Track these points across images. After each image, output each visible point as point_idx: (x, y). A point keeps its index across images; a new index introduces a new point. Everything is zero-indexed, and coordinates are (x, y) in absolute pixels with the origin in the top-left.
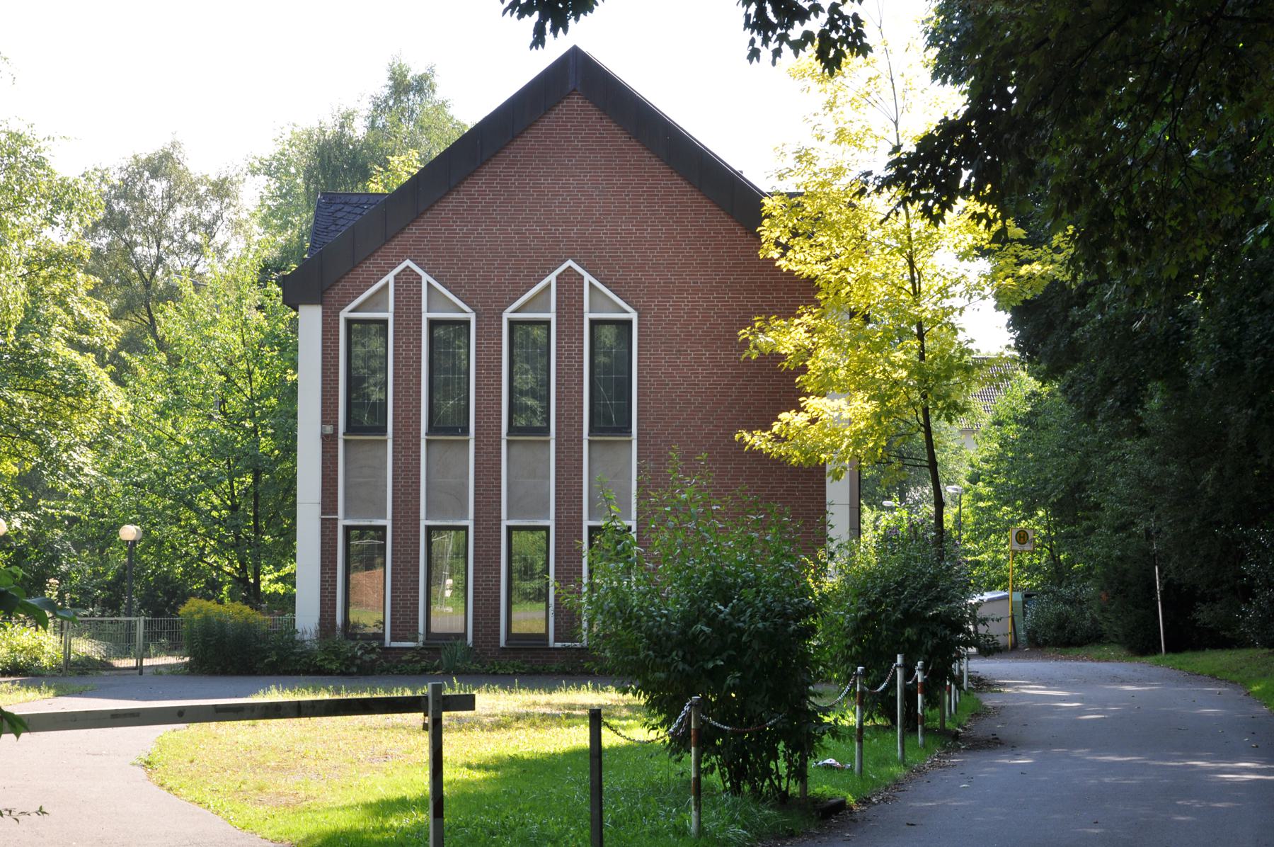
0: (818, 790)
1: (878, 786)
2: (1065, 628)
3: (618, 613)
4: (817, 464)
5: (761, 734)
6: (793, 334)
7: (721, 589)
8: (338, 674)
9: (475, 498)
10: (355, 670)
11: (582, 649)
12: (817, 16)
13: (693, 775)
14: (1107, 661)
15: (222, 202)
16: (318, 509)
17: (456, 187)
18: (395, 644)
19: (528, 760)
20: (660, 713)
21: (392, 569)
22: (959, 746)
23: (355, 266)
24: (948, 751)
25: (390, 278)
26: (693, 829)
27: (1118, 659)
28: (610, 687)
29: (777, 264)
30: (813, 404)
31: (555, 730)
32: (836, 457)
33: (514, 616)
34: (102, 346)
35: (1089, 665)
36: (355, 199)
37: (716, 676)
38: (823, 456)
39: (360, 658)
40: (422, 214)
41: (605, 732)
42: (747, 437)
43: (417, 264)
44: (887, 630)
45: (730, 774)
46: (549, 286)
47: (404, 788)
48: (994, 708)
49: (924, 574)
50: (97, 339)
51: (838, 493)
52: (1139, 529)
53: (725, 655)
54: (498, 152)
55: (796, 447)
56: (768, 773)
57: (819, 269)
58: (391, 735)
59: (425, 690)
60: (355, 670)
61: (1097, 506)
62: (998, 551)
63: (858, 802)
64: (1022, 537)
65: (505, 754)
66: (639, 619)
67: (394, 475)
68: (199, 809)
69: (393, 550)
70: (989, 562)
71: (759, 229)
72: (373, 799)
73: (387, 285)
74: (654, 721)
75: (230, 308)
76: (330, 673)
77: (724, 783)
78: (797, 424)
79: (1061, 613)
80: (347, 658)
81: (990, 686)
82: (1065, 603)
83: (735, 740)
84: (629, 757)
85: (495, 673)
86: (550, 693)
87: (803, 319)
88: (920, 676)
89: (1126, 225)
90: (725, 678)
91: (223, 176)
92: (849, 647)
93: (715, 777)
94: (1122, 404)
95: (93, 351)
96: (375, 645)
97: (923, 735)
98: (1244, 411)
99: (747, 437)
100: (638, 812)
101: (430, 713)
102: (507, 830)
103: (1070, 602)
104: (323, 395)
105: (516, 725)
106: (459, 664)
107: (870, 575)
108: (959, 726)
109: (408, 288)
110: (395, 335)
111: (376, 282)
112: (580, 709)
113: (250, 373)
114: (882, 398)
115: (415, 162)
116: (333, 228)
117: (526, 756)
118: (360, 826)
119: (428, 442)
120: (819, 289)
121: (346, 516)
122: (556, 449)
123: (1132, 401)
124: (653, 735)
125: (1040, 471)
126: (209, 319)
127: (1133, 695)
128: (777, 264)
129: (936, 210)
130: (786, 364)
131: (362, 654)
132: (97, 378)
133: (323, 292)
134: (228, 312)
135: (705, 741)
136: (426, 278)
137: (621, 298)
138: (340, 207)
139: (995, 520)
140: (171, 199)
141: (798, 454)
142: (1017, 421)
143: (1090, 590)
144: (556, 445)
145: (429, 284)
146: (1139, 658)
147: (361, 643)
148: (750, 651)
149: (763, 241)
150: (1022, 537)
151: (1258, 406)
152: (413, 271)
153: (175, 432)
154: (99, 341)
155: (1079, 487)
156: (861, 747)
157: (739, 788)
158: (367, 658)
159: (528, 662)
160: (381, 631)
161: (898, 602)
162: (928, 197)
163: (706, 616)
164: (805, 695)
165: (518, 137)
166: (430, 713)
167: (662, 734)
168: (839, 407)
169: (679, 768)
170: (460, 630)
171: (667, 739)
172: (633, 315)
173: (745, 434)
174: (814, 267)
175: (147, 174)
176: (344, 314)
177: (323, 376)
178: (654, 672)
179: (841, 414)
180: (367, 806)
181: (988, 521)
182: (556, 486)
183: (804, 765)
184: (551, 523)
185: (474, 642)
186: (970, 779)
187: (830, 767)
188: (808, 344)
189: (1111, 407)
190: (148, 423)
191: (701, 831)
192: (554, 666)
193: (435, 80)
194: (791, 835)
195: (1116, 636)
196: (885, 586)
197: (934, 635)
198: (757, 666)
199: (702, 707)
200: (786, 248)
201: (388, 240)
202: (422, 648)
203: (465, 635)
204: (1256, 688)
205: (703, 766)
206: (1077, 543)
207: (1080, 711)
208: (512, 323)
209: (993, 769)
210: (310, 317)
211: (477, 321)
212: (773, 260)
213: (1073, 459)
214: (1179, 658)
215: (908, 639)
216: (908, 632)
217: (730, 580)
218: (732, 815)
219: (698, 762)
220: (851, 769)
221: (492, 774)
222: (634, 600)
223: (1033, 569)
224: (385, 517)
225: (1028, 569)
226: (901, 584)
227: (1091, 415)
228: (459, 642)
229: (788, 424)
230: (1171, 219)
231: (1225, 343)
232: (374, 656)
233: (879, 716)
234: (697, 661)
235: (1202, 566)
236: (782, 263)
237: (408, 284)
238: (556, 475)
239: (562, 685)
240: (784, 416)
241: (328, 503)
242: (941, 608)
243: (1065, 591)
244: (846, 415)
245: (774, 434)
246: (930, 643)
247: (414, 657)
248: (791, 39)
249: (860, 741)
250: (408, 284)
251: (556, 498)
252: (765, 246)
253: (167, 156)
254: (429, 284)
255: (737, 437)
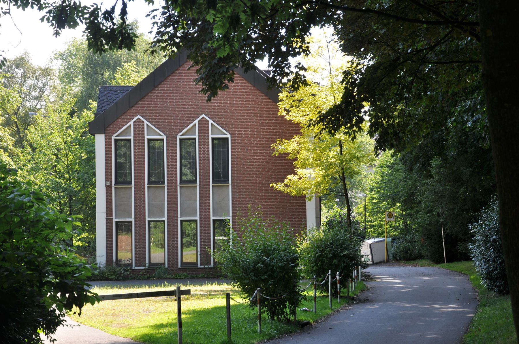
0: (300, 318)
1: (322, 316)
2: (408, 253)
3: (232, 261)
4: (302, 195)
5: (280, 300)
6: (291, 145)
7: (267, 252)
8: (115, 280)
9: (167, 209)
10: (121, 278)
11: (211, 268)
12: (292, 74)
13: (258, 314)
14: (424, 266)
15: (47, 78)
16: (105, 215)
17: (157, 86)
18: (136, 268)
19: (199, 311)
20: (246, 293)
21: (135, 238)
22: (353, 302)
23: (118, 118)
24: (349, 304)
25: (132, 123)
26: (259, 331)
27: (429, 265)
28: (224, 283)
29: (285, 118)
30: (300, 171)
31: (206, 300)
32: (309, 192)
33: (184, 253)
34: (7, 147)
35: (416, 268)
36: (114, 88)
37: (265, 281)
38: (304, 192)
39: (123, 274)
40: (144, 97)
41: (231, 301)
42: (275, 185)
43: (142, 117)
44: (327, 260)
45: (270, 313)
46: (195, 125)
47: (161, 321)
48: (371, 287)
49: (340, 240)
50: (5, 144)
51: (311, 206)
52: (435, 212)
53: (268, 274)
54: (174, 72)
55: (294, 189)
56: (283, 313)
57: (301, 119)
58: (148, 303)
59: (173, 288)
60: (121, 278)
61: (420, 202)
62: (381, 221)
63: (314, 322)
64: (390, 215)
65: (209, 307)
66: (239, 262)
67: (135, 201)
68: (95, 329)
69: (135, 231)
70: (378, 225)
71: (278, 104)
72: (152, 325)
73: (130, 125)
74: (244, 296)
75: (58, 128)
76: (111, 280)
77: (268, 317)
78: (294, 180)
79: (406, 247)
80: (118, 274)
81: (372, 278)
82: (408, 242)
83: (272, 302)
84: (234, 309)
85: (177, 278)
86: (201, 286)
87: (295, 139)
88: (338, 277)
89: (393, 135)
90: (268, 282)
91: (47, 67)
92: (313, 267)
93: (265, 315)
94: (423, 165)
95: (3, 149)
96: (129, 268)
97: (339, 299)
98: (468, 169)
99: (275, 185)
100: (241, 326)
101: (177, 296)
102: (199, 332)
103: (410, 242)
104: (106, 170)
105: (191, 298)
106: (162, 275)
107: (321, 240)
108: (355, 295)
109: (139, 127)
110: (134, 145)
111: (126, 124)
112: (214, 292)
113: (67, 155)
114: (326, 169)
115: (134, 66)
116: (106, 100)
117: (198, 310)
118: (152, 332)
119: (148, 187)
120: (302, 127)
121: (116, 217)
122: (199, 189)
123: (426, 165)
124: (244, 301)
125: (397, 188)
126: (49, 132)
127: (425, 281)
128: (285, 118)
129: (333, 132)
130: (289, 157)
131: (124, 272)
132: (6, 160)
133: (105, 129)
134: (57, 130)
135: (262, 302)
136: (146, 122)
137: (224, 129)
138: (108, 91)
139: (380, 208)
140: (25, 77)
141: (294, 192)
142: (387, 166)
143: (418, 237)
144: (199, 188)
145: (147, 125)
146: (436, 265)
147: (124, 267)
148: (276, 272)
149: (279, 108)
150: (390, 215)
151: (473, 167)
152: (141, 120)
153: (34, 179)
154: (6, 144)
155: (413, 194)
156: (315, 303)
157: (273, 318)
158: (126, 273)
159: (190, 273)
160: (130, 263)
161: (331, 250)
162: (330, 127)
163: (261, 261)
164: (295, 287)
165: (181, 66)
166: (177, 296)
167: (247, 301)
168: (310, 173)
169: (253, 312)
170: (162, 262)
171: (249, 302)
172: (229, 136)
173: (274, 184)
174: (300, 118)
175: (14, 67)
176: (114, 137)
177: (106, 162)
178: (244, 280)
179: (311, 175)
180: (151, 326)
181: (377, 208)
182: (200, 204)
183: (295, 309)
184: (198, 218)
185: (168, 266)
186: (354, 314)
187: (305, 310)
188: (297, 148)
189: (419, 167)
190: (24, 176)
191: (261, 331)
192: (200, 275)
193: (138, 25)
194: (291, 332)
195: (427, 256)
196: (326, 245)
197: (344, 262)
198: (279, 277)
199: (261, 291)
200: (288, 111)
201: (130, 108)
202: (148, 269)
203: (164, 264)
204: (472, 277)
205: (261, 311)
206: (412, 218)
207: (402, 288)
208: (181, 140)
209: (363, 310)
210: (100, 140)
211: (167, 139)
212: (284, 116)
213: (410, 183)
214: (451, 265)
215: (335, 264)
216: (335, 261)
217: (269, 248)
218: (271, 326)
219: (260, 310)
220: (312, 311)
221: (188, 316)
222: (238, 256)
223: (397, 228)
224: (131, 218)
225: (394, 228)
226: (331, 244)
227: (411, 170)
228: (162, 266)
229: (290, 180)
230: (407, 132)
231: (460, 143)
232: (129, 273)
233: (325, 292)
234: (259, 276)
235: (460, 227)
236: (287, 117)
237: (139, 125)
238: (200, 200)
239: (205, 283)
240: (289, 177)
241: (109, 212)
242: (346, 252)
243: (408, 237)
244: (313, 176)
245: (285, 184)
246: (342, 265)
247: (144, 273)
248: (283, 82)
249: (315, 301)
250: (139, 125)
251: (200, 209)
252: (280, 110)
253: (23, 59)
254: (147, 125)
255: (271, 185)
